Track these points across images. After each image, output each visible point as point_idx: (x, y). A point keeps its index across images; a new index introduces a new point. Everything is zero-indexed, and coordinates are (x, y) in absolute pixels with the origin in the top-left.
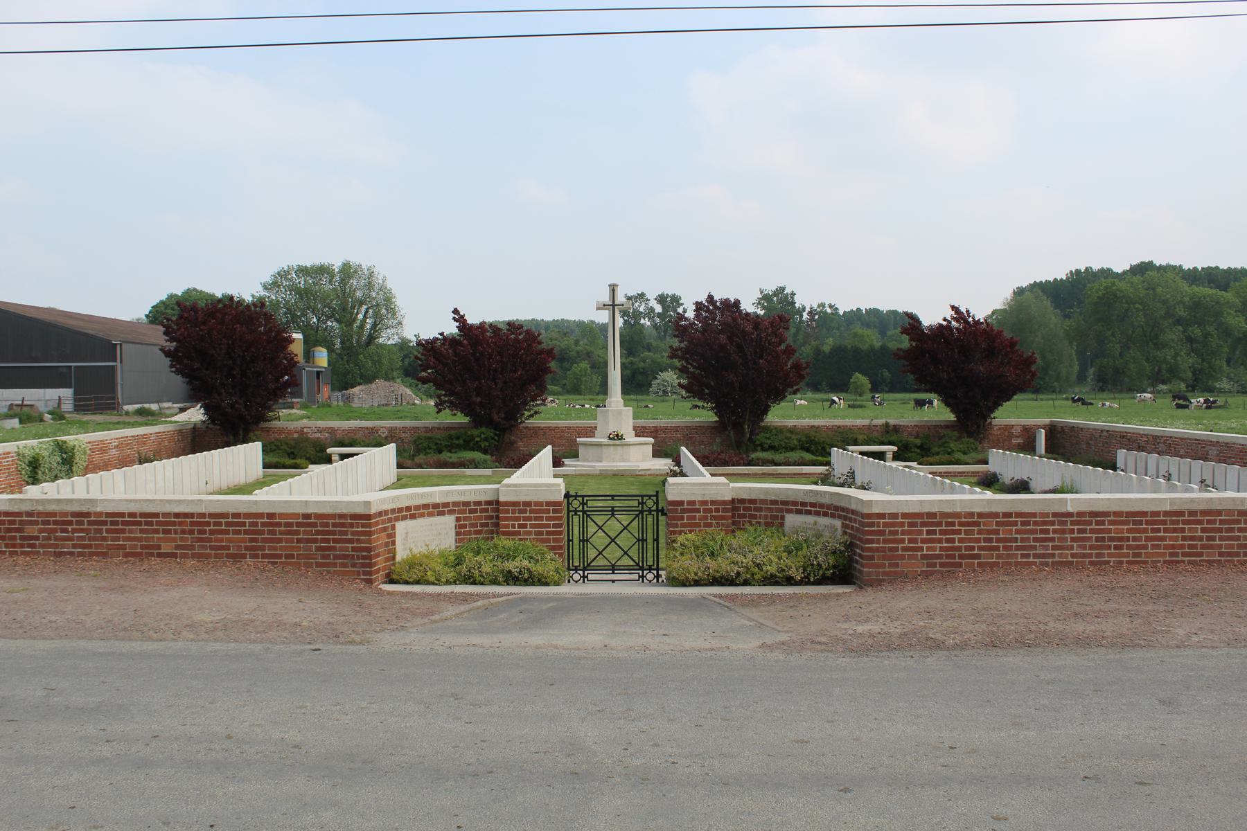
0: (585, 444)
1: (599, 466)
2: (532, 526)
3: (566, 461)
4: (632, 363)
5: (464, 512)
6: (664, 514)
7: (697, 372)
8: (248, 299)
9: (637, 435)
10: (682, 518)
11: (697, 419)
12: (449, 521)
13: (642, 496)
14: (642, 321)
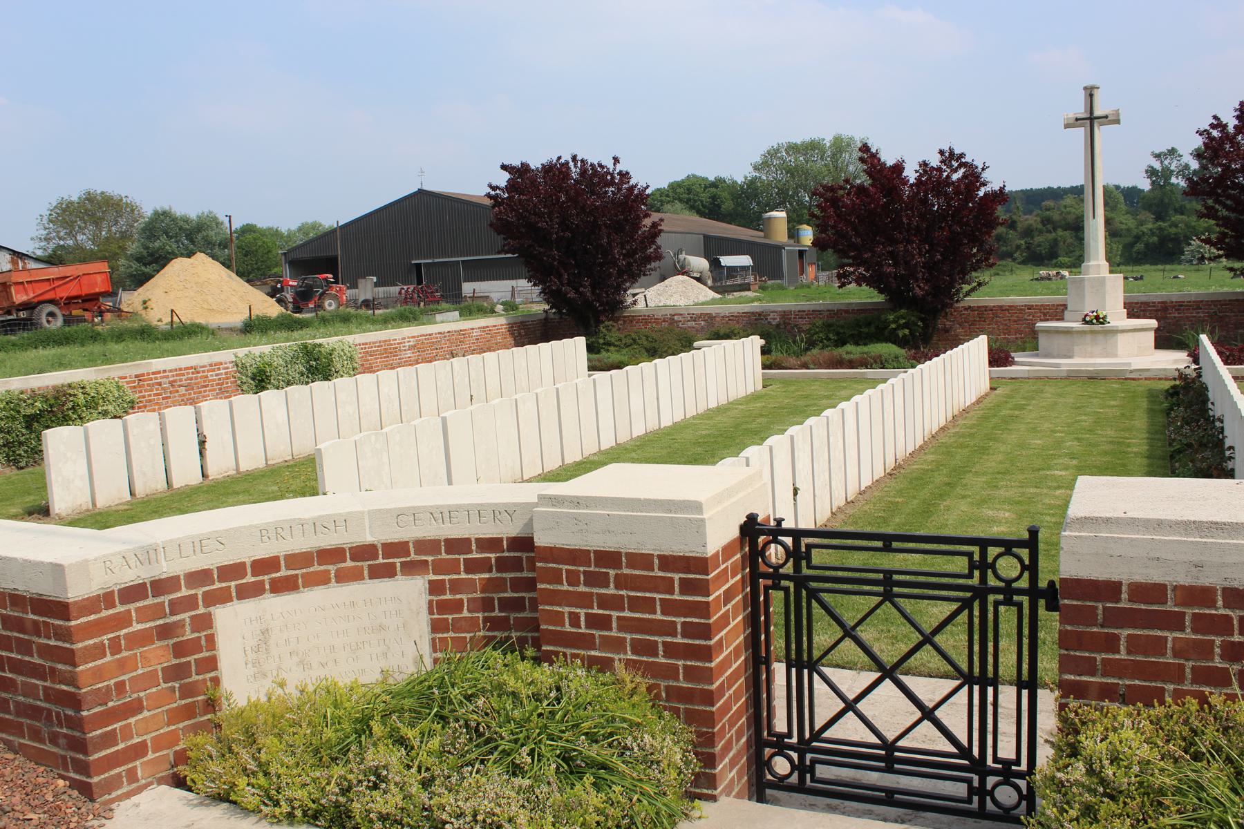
0: (1048, 331)
1: (1066, 364)
2: (625, 624)
3: (1018, 357)
4: (1160, 229)
5: (452, 567)
6: (1052, 606)
7: (1233, 215)
8: (740, 180)
9: (1131, 315)
10: (1111, 644)
11: (1226, 289)
12: (409, 594)
13: (984, 544)
14: (1173, 180)
